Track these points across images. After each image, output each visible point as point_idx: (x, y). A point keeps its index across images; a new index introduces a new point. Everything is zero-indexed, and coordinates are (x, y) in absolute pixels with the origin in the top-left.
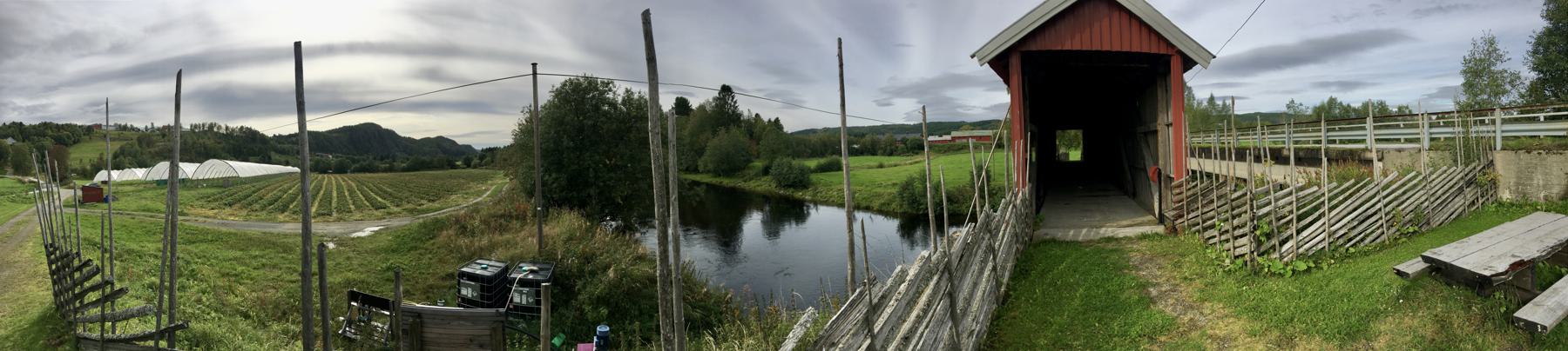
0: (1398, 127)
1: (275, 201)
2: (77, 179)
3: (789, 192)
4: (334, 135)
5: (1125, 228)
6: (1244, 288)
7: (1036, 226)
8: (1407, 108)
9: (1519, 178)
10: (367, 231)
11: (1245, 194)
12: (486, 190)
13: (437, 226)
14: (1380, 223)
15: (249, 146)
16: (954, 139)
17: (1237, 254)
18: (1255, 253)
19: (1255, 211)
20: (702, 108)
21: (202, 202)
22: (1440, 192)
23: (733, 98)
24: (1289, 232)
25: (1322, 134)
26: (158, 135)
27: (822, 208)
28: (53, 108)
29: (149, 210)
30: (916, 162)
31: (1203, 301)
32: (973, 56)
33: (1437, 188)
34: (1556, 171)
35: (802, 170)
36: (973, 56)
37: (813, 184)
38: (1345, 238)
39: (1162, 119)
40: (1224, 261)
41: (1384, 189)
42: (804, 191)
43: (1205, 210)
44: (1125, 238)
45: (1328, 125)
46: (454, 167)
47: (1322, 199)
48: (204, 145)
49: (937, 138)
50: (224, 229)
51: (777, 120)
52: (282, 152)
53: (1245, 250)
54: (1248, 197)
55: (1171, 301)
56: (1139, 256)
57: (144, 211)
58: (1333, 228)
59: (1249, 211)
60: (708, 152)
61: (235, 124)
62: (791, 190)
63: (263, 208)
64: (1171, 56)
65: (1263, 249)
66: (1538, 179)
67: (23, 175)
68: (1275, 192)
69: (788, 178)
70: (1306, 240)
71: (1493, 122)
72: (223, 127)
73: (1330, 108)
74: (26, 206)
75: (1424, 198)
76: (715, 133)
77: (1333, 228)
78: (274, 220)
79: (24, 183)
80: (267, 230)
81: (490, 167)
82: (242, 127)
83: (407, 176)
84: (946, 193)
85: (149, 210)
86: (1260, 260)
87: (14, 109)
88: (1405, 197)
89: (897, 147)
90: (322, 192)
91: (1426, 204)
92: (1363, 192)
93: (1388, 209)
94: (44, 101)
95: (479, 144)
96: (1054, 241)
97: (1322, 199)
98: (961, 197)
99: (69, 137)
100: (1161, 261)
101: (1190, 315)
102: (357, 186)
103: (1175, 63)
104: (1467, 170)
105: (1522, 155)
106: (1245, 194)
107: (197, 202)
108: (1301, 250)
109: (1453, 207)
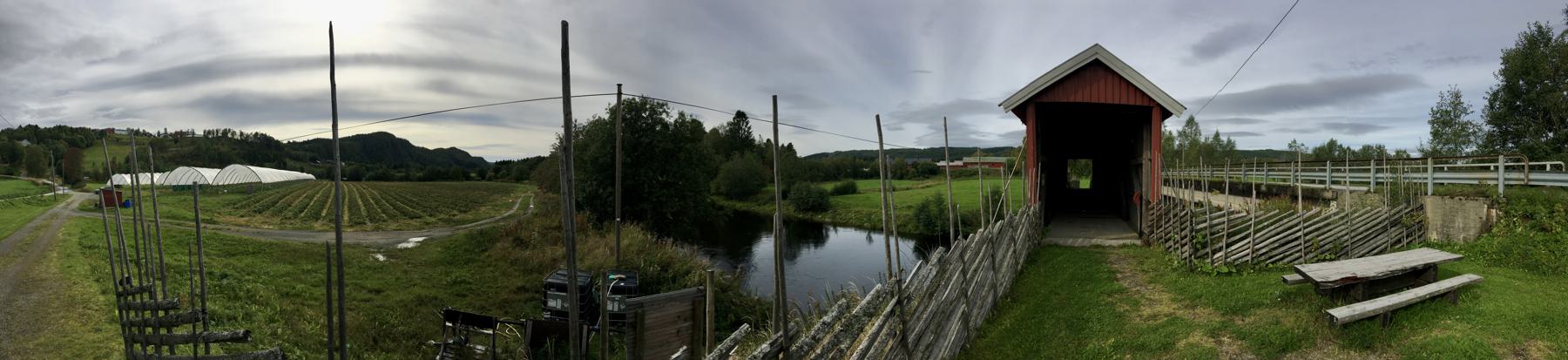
0: (1314, 171)
1: (305, 208)
2: (90, 182)
3: (808, 216)
4: (348, 142)
5: (1112, 240)
7: (1043, 234)
8: (1405, 152)
9: (1444, 221)
10: (413, 241)
11: (1187, 213)
12: (514, 203)
13: (484, 239)
14: (1299, 248)
15: (263, 151)
20: (715, 131)
21: (227, 210)
22: (1362, 229)
23: (747, 123)
24: (1220, 244)
25: (1327, 174)
26: (171, 141)
27: (841, 230)
28: (63, 112)
29: (174, 217)
30: (928, 187)
31: (1150, 283)
32: (1000, 105)
33: (1358, 225)
34: (1473, 216)
35: (821, 194)
36: (1000, 105)
37: (832, 207)
38: (1267, 256)
39: (1146, 155)
41: (1305, 221)
42: (824, 213)
45: (1333, 165)
46: (468, 178)
47: (1249, 223)
48: (217, 150)
50: (263, 239)
51: (790, 145)
52: (297, 159)
57: (168, 217)
58: (1257, 247)
60: (721, 175)
61: (250, 131)
62: (811, 213)
63: (296, 216)
64: (1153, 107)
65: (1199, 254)
66: (1459, 222)
67: (36, 178)
68: (1210, 213)
69: (807, 203)
70: (1234, 252)
71: (1497, 168)
72: (238, 133)
73: (1331, 151)
74: (41, 209)
75: (1344, 232)
76: (728, 156)
77: (1257, 247)
78: (311, 229)
79: (37, 184)
80: (311, 240)
81: (506, 180)
82: (257, 133)
83: (428, 185)
84: (961, 217)
85: (174, 217)
86: (1196, 261)
87: (27, 112)
88: (1326, 229)
89: (908, 171)
90: (347, 200)
91: (1346, 237)
92: (1285, 221)
93: (1307, 238)
94: (56, 105)
95: (492, 156)
96: (1056, 245)
97: (1249, 223)
98: (975, 221)
99: (82, 140)
102: (380, 194)
103: (1156, 115)
104: (1393, 212)
105: (1448, 200)
107: (223, 210)
108: (1229, 260)
109: (1375, 243)
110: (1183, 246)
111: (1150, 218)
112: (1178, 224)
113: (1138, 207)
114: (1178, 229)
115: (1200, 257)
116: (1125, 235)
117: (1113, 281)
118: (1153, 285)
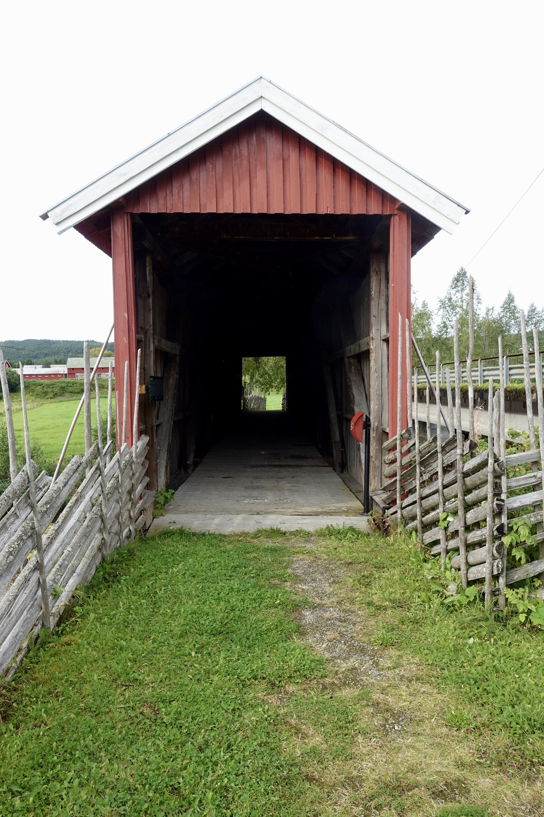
6: (471, 641)
11: (484, 464)
16: (72, 372)
17: (471, 577)
18: (502, 581)
19: (503, 497)
31: (386, 644)
32: (45, 217)
40: (445, 587)
43: (427, 491)
44: (297, 533)
49: (39, 370)
53: (483, 571)
54: (490, 467)
55: (330, 635)
56: (308, 559)
59: (490, 495)
86: (510, 594)
100: (341, 572)
101: (353, 662)
106: (484, 464)
110: (470, 547)
111: (387, 470)
112: (457, 488)
113: (362, 445)
114: (458, 503)
115: (521, 584)
116: (333, 507)
117: (288, 637)
118: (393, 652)
